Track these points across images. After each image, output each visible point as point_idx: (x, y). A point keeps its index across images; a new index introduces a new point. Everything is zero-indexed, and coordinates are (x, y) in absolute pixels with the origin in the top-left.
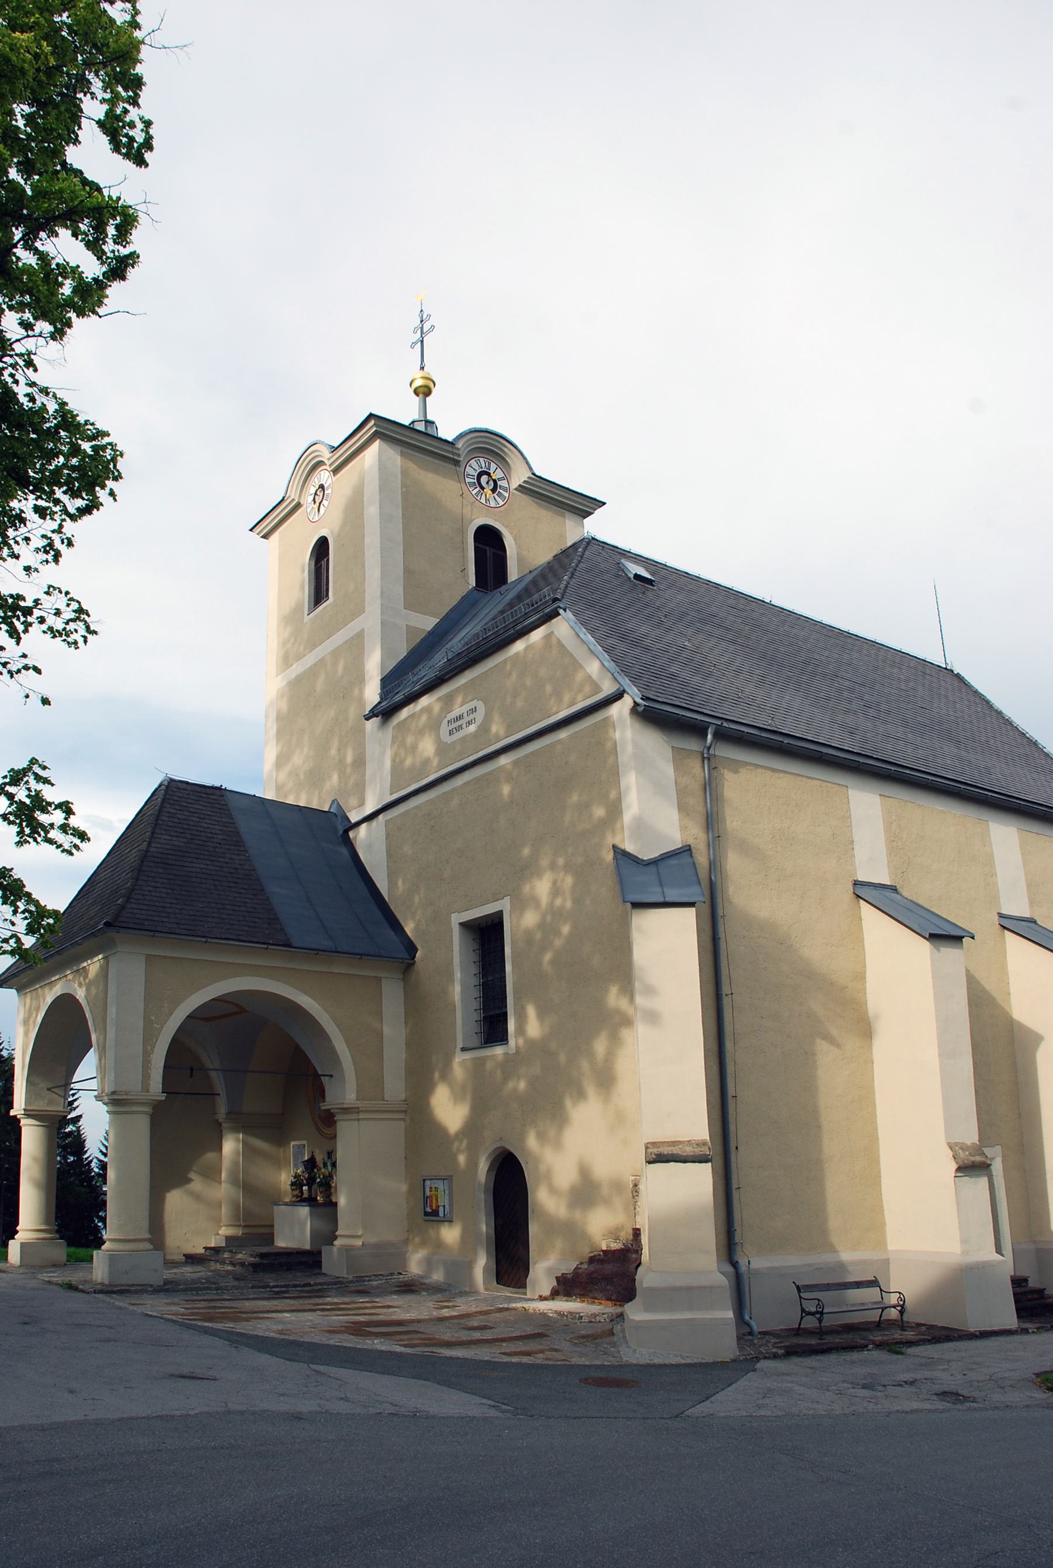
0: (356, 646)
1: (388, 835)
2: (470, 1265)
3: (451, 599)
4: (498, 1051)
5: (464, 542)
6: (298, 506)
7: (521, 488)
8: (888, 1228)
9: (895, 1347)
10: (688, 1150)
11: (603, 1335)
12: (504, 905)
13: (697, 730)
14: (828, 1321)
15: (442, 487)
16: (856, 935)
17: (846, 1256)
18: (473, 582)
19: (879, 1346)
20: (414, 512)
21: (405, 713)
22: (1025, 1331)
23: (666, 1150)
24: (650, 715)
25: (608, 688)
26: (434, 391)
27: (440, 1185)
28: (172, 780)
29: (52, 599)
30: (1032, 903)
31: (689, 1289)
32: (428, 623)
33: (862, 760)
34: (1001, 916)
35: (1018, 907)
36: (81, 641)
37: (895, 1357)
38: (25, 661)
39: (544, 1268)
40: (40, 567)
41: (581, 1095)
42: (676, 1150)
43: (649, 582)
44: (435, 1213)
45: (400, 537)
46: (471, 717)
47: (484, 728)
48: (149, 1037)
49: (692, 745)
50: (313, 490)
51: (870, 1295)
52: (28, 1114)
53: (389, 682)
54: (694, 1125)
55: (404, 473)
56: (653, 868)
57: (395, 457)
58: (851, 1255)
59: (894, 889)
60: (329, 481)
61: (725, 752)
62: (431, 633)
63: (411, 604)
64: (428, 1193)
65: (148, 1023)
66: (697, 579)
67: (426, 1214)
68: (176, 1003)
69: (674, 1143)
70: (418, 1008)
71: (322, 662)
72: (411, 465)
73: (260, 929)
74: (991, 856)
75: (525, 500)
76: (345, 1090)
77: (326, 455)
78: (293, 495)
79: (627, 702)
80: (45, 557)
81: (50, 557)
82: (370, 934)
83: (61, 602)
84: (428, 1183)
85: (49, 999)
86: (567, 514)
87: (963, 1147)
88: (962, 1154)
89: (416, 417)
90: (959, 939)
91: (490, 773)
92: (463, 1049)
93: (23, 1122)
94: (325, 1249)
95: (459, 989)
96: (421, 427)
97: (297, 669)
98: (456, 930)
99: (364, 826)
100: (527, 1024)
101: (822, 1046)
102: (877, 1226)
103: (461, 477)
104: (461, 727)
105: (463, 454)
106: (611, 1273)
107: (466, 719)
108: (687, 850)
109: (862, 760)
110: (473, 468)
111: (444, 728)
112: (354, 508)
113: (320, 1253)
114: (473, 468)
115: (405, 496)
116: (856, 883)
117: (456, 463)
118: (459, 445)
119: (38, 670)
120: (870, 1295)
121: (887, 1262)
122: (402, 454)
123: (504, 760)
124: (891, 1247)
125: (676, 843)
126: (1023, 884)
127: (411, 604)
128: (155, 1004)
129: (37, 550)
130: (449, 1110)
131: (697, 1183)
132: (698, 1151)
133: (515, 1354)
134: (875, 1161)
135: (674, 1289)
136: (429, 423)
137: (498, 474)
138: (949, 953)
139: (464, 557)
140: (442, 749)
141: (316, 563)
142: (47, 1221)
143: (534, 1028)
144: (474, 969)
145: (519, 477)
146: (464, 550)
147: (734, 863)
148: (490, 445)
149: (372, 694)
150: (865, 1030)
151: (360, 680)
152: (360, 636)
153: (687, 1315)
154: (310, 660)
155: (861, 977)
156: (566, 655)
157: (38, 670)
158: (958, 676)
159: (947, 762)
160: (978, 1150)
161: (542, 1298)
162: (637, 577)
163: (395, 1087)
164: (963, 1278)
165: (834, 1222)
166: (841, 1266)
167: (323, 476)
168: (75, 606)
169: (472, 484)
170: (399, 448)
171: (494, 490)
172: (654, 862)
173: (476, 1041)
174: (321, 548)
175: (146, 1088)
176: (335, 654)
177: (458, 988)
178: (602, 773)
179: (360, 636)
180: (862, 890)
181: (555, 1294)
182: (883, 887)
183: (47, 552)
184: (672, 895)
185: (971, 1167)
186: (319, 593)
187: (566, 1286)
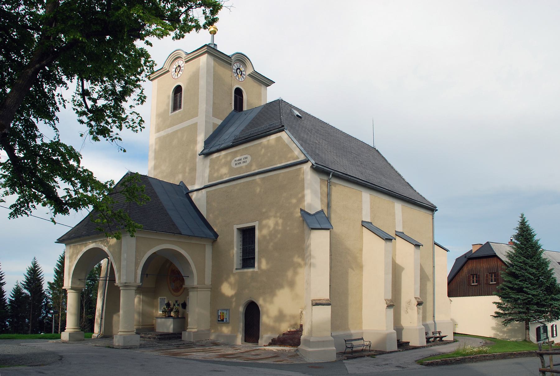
0: (194, 127)
1: (207, 197)
2: (235, 337)
3: (226, 114)
4: (251, 270)
5: (231, 93)
6: (168, 71)
7: (249, 75)
8: (363, 324)
9: (373, 356)
10: (324, 302)
11: (295, 355)
12: (256, 224)
13: (327, 173)
14: (354, 349)
15: (225, 72)
16: (361, 238)
17: (352, 331)
18: (233, 108)
19: (368, 356)
20: (217, 82)
21: (215, 155)
22: (400, 351)
23: (318, 302)
24: (317, 169)
25: (302, 158)
26: (217, 32)
27: (225, 312)
28: (131, 173)
29: (132, 115)
30: (403, 227)
31: (323, 341)
32: (219, 122)
33: (349, 177)
34: (396, 231)
35: (400, 229)
36: (139, 130)
37: (372, 359)
38: (117, 136)
39: (265, 337)
40: (135, 106)
41: (281, 286)
42: (321, 302)
43: (300, 117)
44: (223, 320)
45: (212, 91)
46: (245, 160)
47: (250, 165)
48: (137, 264)
49: (325, 178)
50: (175, 67)
51: (361, 342)
52: (72, 288)
53: (207, 143)
54: (325, 295)
55: (214, 68)
56: (314, 217)
57: (212, 61)
58: (354, 331)
59: (371, 223)
60: (183, 65)
61: (334, 180)
62: (220, 126)
63: (215, 115)
64: (219, 314)
65: (136, 259)
66: (309, 115)
67: (218, 321)
68: (145, 253)
69: (320, 300)
70: (217, 256)
71: (176, 132)
72: (217, 65)
73: (172, 229)
74: (395, 213)
75: (250, 79)
76: (193, 281)
77: (184, 55)
78: (167, 67)
79: (309, 165)
80: (138, 102)
81: (139, 102)
82: (203, 230)
83: (135, 116)
84: (220, 311)
85: (85, 249)
86: (262, 85)
87: (388, 300)
88: (388, 302)
89: (210, 42)
90: (392, 240)
91: (253, 180)
92: (236, 269)
93: (68, 291)
94: (183, 332)
95: (236, 252)
96: (213, 46)
97: (162, 133)
98: (235, 232)
99: (195, 193)
100: (262, 264)
101: (350, 270)
102: (361, 323)
103: (232, 69)
104: (240, 163)
105: (233, 61)
106: (292, 338)
107: (243, 160)
108: (322, 211)
109: (349, 177)
110: (235, 66)
111: (233, 164)
112: (194, 79)
113: (181, 334)
114: (235, 66)
115: (214, 75)
116: (362, 222)
117: (231, 64)
118: (232, 58)
119: (120, 139)
120: (361, 342)
121: (363, 333)
122: (214, 60)
123: (257, 177)
124: (364, 329)
125: (319, 209)
126: (401, 221)
127: (215, 115)
128: (139, 253)
129: (135, 100)
130: (227, 290)
131: (325, 313)
132: (327, 302)
133: (278, 361)
134: (361, 304)
135: (319, 342)
136: (215, 45)
137: (242, 69)
138: (389, 243)
139: (231, 99)
140: (231, 170)
141: (175, 94)
142: (77, 325)
143: (264, 265)
144: (241, 243)
145: (249, 71)
146: (231, 96)
147: (333, 216)
148: (242, 59)
149: (200, 147)
150: (361, 267)
151: (195, 142)
152: (195, 125)
153: (320, 349)
154: (170, 130)
155: (361, 250)
156: (284, 144)
157: (120, 139)
158: (377, 150)
159: (384, 183)
160: (391, 301)
161: (265, 346)
162: (297, 116)
163: (208, 281)
164: (385, 339)
165: (350, 322)
166: (351, 335)
167: (181, 62)
168: (140, 118)
169: (234, 72)
170: (213, 58)
171: (241, 75)
172: (314, 215)
173: (240, 266)
174: (178, 90)
175: (135, 281)
176: (182, 130)
177: (235, 249)
178: (299, 187)
179: (195, 125)
180: (364, 224)
181: (270, 344)
182: (369, 222)
183: (138, 100)
184: (323, 227)
185: (389, 306)
186: (176, 105)
187: (274, 342)
